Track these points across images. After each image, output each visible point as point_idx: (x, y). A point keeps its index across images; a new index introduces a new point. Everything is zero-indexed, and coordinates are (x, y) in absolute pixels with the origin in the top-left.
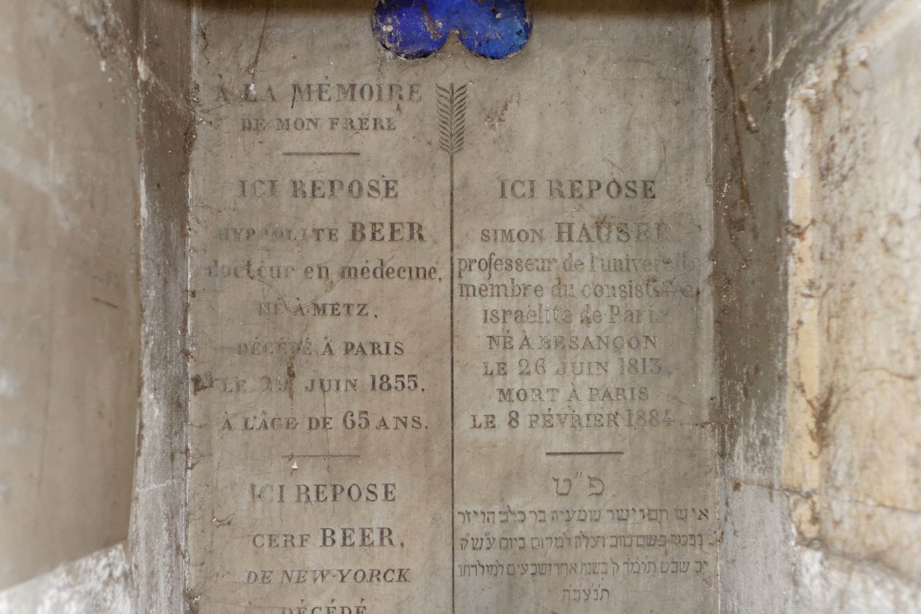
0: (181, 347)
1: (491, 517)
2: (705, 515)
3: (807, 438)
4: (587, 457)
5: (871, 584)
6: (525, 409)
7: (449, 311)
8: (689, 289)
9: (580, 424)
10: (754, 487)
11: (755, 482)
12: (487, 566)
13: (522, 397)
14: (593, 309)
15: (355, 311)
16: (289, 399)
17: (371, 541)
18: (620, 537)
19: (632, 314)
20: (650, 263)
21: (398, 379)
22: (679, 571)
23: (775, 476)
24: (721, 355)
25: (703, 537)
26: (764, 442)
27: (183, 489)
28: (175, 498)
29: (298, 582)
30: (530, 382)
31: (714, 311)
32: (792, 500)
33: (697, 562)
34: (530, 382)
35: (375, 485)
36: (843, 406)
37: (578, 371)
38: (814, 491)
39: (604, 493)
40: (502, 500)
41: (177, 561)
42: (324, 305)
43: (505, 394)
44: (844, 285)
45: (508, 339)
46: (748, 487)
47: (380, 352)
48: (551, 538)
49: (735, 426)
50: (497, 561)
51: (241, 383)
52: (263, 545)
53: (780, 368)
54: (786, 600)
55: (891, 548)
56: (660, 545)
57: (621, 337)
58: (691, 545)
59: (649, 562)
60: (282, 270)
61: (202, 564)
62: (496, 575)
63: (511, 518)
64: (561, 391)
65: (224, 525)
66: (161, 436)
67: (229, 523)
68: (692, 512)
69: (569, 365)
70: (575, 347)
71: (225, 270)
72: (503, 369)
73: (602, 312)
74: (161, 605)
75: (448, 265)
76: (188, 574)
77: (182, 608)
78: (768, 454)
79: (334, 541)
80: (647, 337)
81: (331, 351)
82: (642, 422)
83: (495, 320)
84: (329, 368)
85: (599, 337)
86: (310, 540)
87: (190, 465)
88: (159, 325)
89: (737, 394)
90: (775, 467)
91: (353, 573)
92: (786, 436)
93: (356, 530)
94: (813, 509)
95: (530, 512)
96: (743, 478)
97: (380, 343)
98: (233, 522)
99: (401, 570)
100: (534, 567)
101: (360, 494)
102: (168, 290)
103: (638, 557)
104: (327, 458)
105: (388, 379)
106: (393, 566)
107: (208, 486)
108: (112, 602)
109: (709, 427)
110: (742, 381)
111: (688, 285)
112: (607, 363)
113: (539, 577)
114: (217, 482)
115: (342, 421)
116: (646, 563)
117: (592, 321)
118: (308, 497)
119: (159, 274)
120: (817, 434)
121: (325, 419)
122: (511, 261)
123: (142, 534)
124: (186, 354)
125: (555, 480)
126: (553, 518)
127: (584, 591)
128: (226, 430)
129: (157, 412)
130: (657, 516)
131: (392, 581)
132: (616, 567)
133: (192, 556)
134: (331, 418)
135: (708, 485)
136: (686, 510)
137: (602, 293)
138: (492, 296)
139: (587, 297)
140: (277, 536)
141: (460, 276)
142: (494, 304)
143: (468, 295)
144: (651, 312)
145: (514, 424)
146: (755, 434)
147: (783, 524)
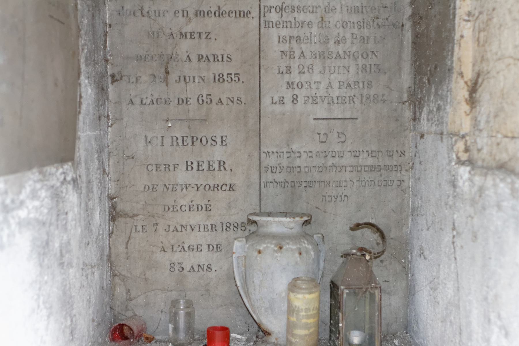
0: (103, 56)
1: (282, 154)
2: (404, 154)
3: (464, 104)
4: (337, 121)
5: (498, 180)
6: (302, 94)
7: (258, 37)
8: (397, 24)
9: (333, 102)
10: (432, 135)
11: (433, 132)
12: (279, 182)
13: (300, 87)
14: (341, 35)
15: (204, 36)
16: (166, 86)
17: (214, 168)
18: (355, 166)
19: (364, 38)
20: (375, 9)
21: (229, 76)
22: (388, 185)
23: (444, 127)
24: (415, 62)
25: (402, 166)
26: (439, 109)
27: (106, 137)
28: (102, 142)
29: (172, 191)
30: (305, 77)
31: (412, 36)
32: (454, 139)
33: (398, 180)
34: (305, 77)
35: (216, 137)
36: (485, 82)
37: (332, 71)
38: (467, 134)
39: (346, 142)
40: (288, 145)
41: (104, 178)
42: (186, 33)
43: (290, 85)
44: (488, 10)
45: (292, 53)
46: (428, 136)
47: (218, 60)
48: (316, 167)
49: (422, 102)
50: (285, 179)
51: (138, 78)
52: (152, 170)
53: (449, 64)
54: (449, 197)
55: (510, 160)
56: (377, 171)
57: (357, 52)
58: (395, 171)
59: (371, 180)
60: (161, 12)
61: (118, 181)
62: (284, 187)
63: (293, 155)
64: (322, 83)
65: (130, 159)
66: (92, 105)
67: (133, 158)
68: (396, 153)
69: (327, 68)
70: (331, 57)
71: (128, 12)
72: (289, 70)
73: (347, 37)
74: (95, 200)
75: (258, 9)
76: (110, 186)
77: (107, 204)
78: (441, 115)
79: (192, 168)
80: (373, 52)
81: (190, 60)
82: (369, 101)
83: (284, 41)
84: (189, 70)
85: (345, 52)
86: (180, 167)
87: (110, 124)
88: (90, 40)
89: (424, 83)
90: (445, 122)
91: (203, 186)
92: (451, 103)
93: (205, 162)
94: (466, 144)
95: (304, 152)
96: (426, 131)
97: (218, 55)
98: (135, 157)
99: (231, 184)
100: (306, 183)
101: (207, 141)
102: (95, 21)
103: (365, 178)
104: (188, 121)
105: (223, 76)
106: (226, 182)
107: (120, 137)
108: (66, 194)
109: (407, 104)
110: (427, 75)
111: (397, 22)
112: (349, 67)
113: (309, 189)
114: (126, 134)
115: (196, 100)
116: (369, 181)
117: (341, 42)
118: (178, 143)
119: (89, 11)
120: (470, 100)
121: (187, 99)
122: (294, 7)
123: (83, 159)
124: (107, 61)
125: (318, 134)
126: (317, 156)
127: (334, 196)
128: (130, 105)
129: (90, 91)
130: (376, 154)
131: (225, 190)
132: (352, 183)
133: (112, 176)
134: (190, 98)
135: (406, 137)
136: (393, 151)
137: (347, 26)
138: (283, 27)
139: (338, 28)
140: (160, 165)
141: (264, 16)
142: (284, 32)
143: (269, 27)
144: (375, 37)
145: (295, 102)
146: (433, 105)
147: (448, 154)
